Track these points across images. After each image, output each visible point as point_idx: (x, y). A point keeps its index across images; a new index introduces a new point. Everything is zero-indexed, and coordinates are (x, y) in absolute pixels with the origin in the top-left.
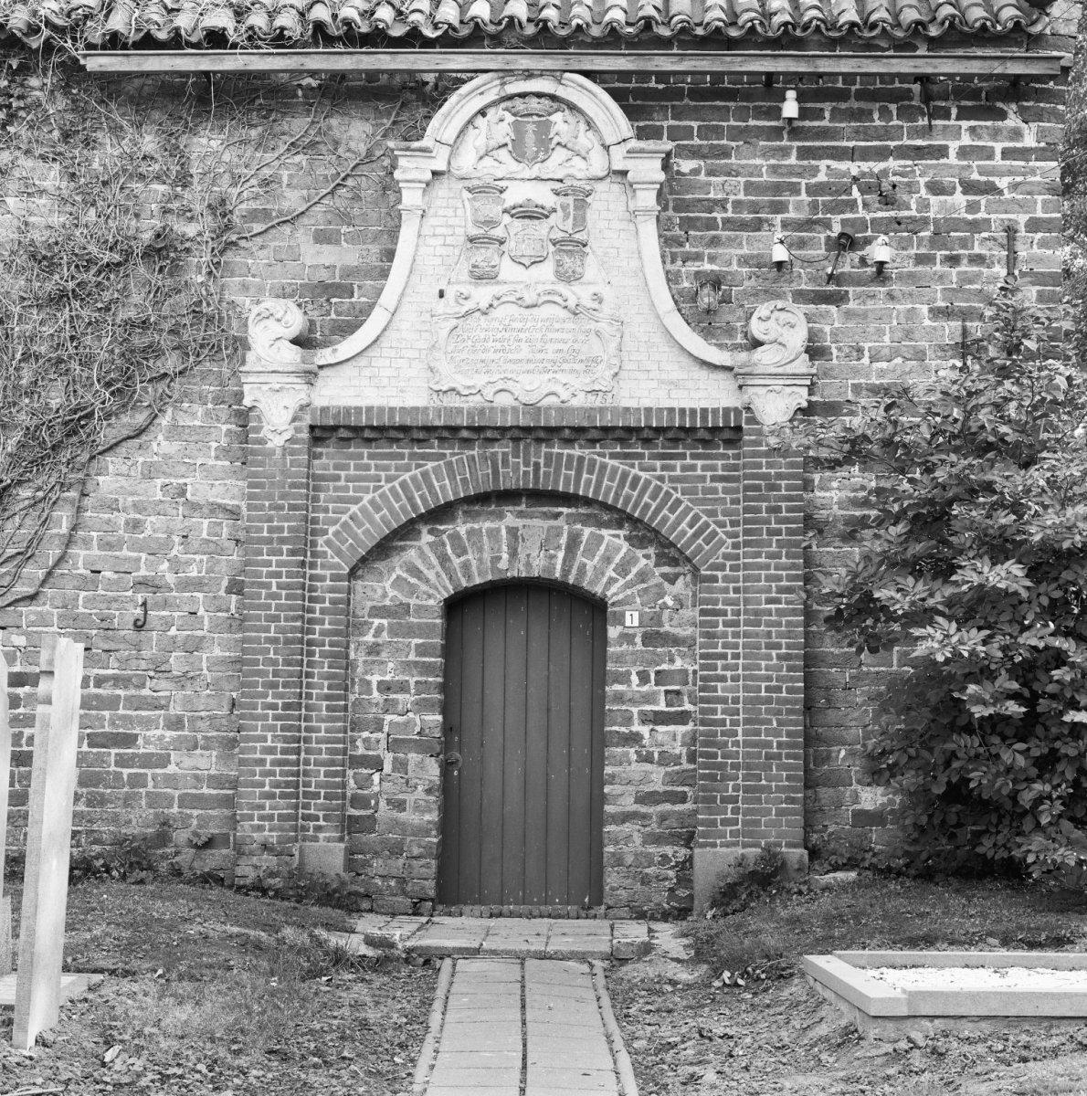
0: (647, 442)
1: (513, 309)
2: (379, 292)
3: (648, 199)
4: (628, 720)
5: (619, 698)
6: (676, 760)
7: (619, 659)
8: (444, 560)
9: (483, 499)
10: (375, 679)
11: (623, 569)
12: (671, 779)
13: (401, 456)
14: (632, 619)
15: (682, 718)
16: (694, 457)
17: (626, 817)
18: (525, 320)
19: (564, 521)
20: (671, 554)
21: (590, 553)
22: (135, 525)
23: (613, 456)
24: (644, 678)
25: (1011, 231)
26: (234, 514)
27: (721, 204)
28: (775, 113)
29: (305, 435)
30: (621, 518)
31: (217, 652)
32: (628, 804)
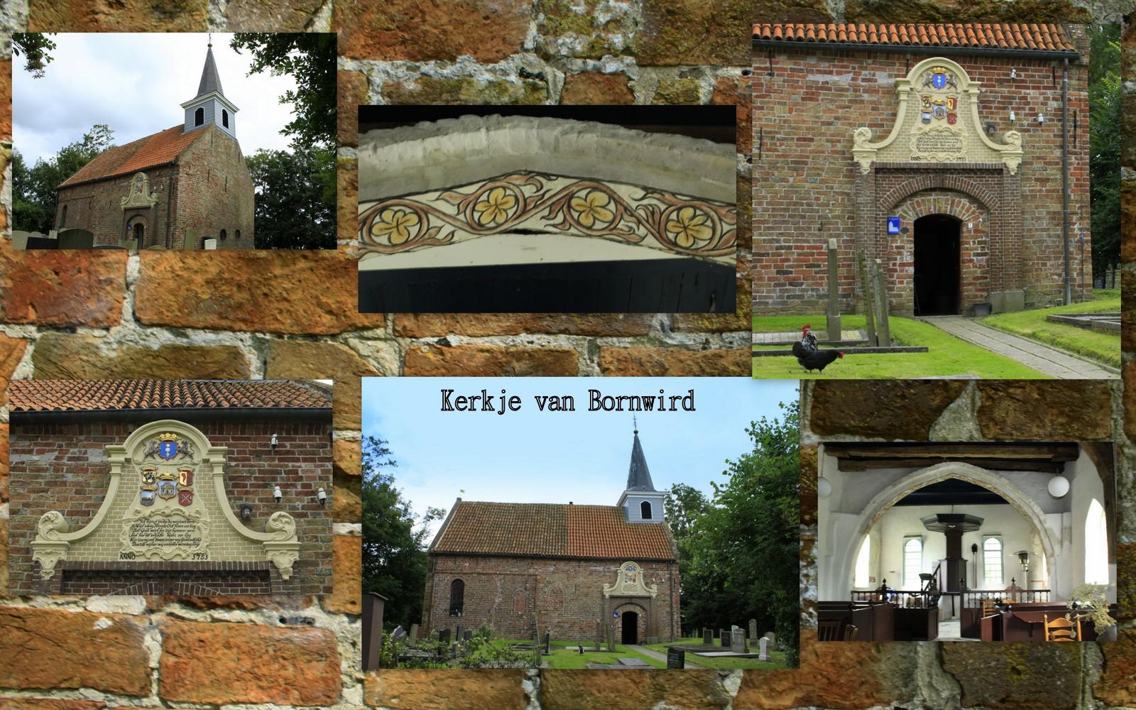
0: (975, 173)
1: (161, 518)
2: (893, 126)
3: (219, 470)
4: (970, 255)
5: (967, 249)
6: (984, 267)
7: (967, 237)
8: (914, 208)
9: (926, 190)
10: (894, 245)
11: (968, 211)
12: (982, 272)
13: (106, 586)
14: (971, 225)
15: (985, 254)
16: (246, 585)
17: (970, 284)
18: (165, 522)
19: (950, 196)
20: (982, 206)
21: (957, 206)
22: (817, 199)
23: (208, 585)
24: (974, 243)
25: (1075, 112)
26: (848, 194)
27: (994, 102)
28: (1008, 75)
29: (60, 574)
30: (967, 196)
31: (845, 238)
32: (971, 280)
